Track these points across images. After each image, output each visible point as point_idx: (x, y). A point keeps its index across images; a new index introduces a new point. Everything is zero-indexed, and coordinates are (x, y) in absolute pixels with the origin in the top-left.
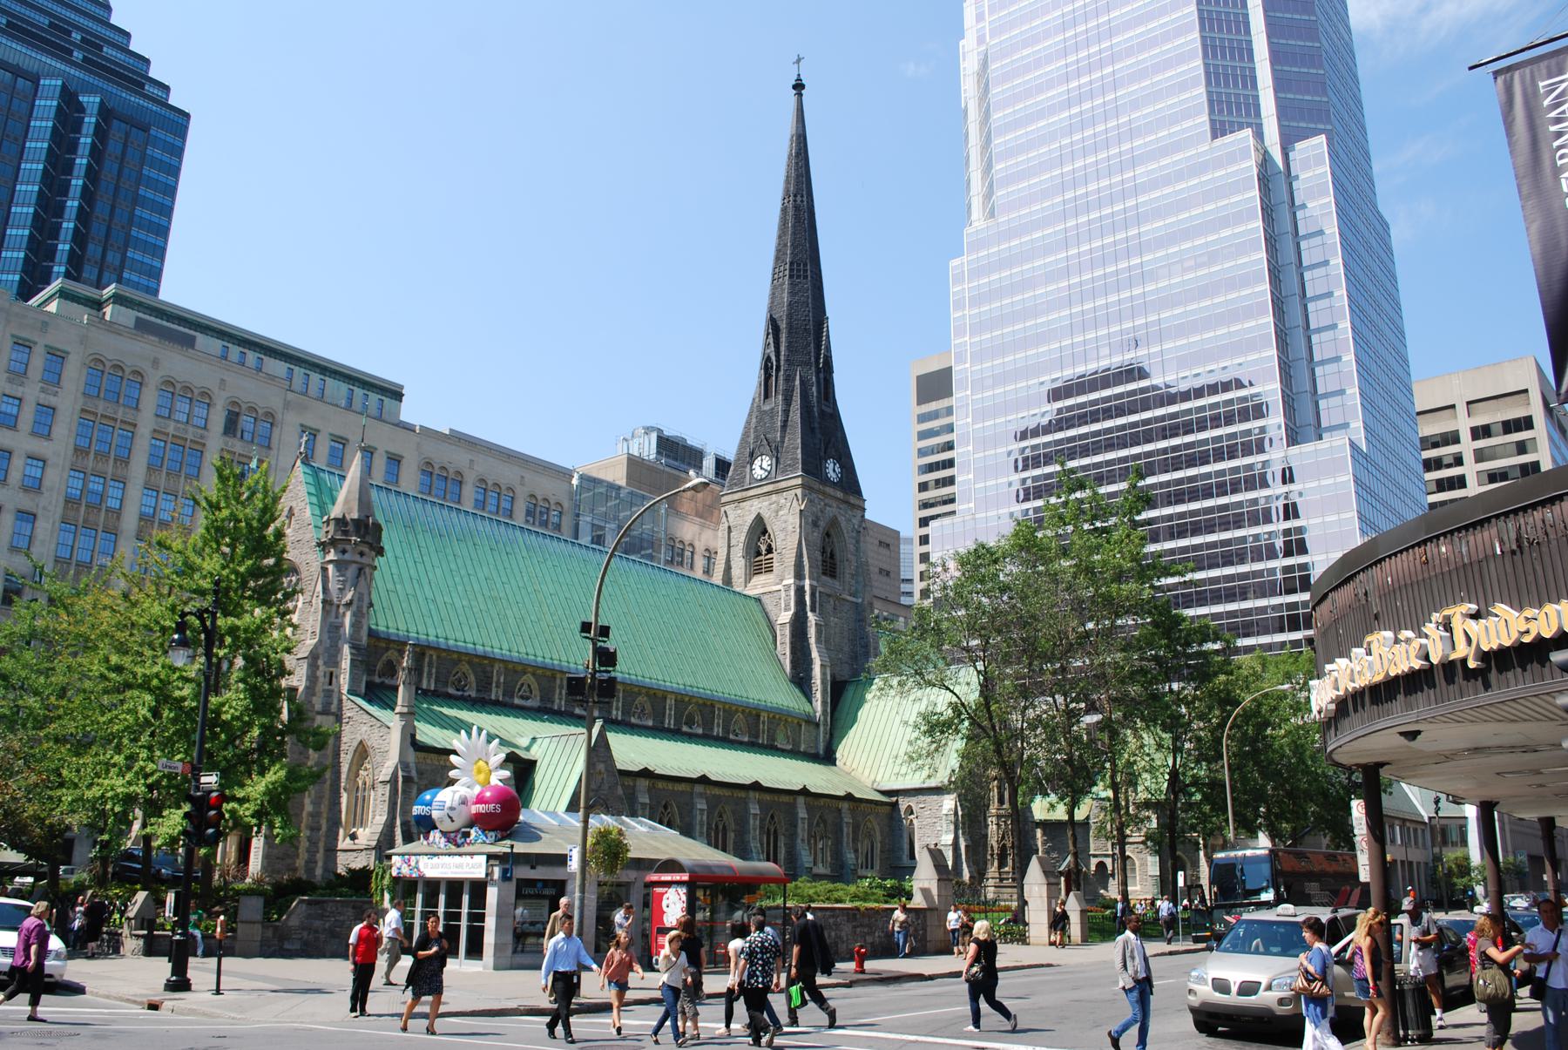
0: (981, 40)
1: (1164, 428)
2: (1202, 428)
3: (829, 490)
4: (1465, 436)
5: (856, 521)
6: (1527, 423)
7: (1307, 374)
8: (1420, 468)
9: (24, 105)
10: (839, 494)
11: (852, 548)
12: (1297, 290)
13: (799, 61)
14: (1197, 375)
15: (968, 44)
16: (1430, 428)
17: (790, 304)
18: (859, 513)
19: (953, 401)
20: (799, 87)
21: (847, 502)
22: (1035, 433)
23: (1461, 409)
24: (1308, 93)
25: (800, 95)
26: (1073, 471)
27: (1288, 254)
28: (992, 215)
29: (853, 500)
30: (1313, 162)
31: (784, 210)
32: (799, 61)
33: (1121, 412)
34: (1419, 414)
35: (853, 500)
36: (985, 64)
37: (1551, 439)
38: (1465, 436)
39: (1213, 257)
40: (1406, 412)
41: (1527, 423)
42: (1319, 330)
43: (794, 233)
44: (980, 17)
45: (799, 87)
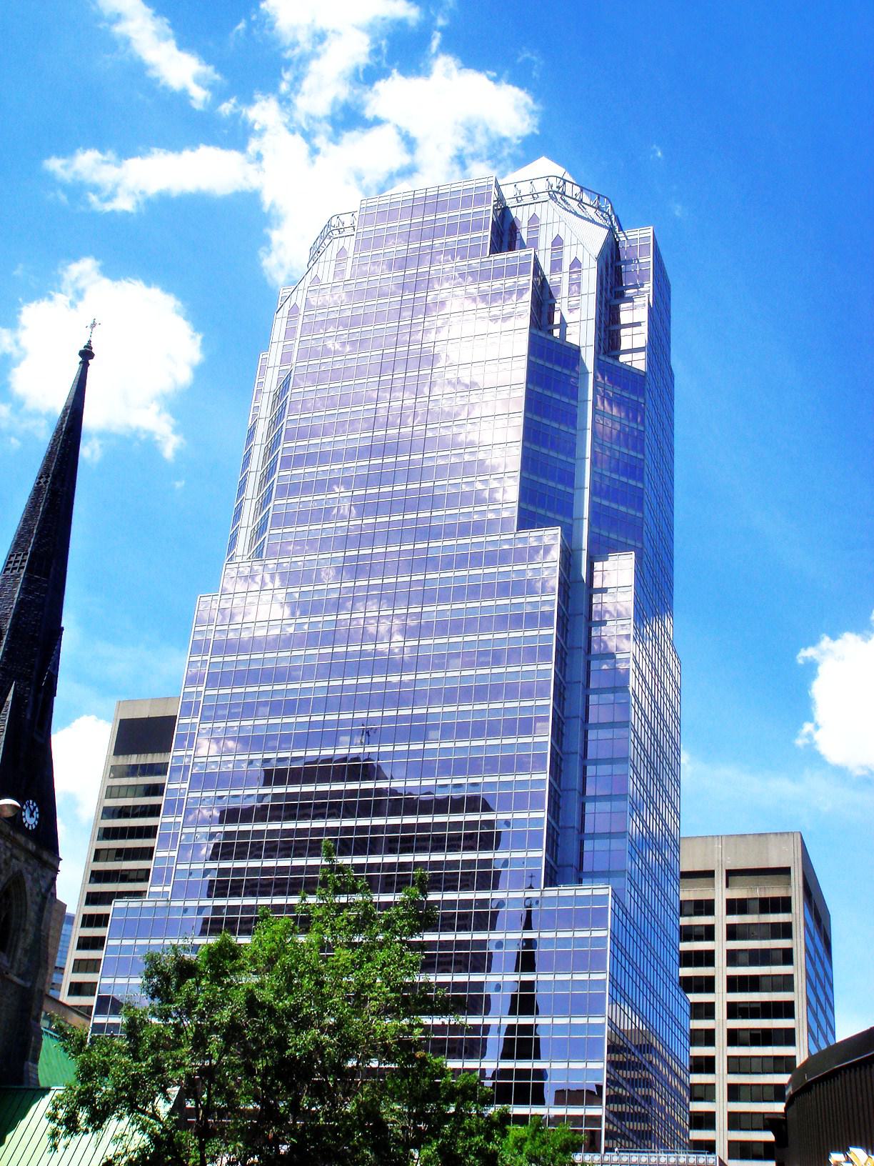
0: (286, 358)
1: (394, 840)
2: (454, 848)
3: (21, 838)
4: (720, 907)
5: (43, 884)
6: (783, 905)
7: (577, 806)
8: (676, 936)
9: (488, 368)
10: (31, 846)
11: (32, 915)
12: (581, 712)
13: (93, 325)
14: (459, 786)
15: (274, 355)
16: (691, 893)
17: (21, 604)
18: (50, 874)
19: (169, 759)
20: (87, 355)
21: (39, 858)
22: (246, 815)
23: (720, 878)
24: (623, 504)
25: (85, 366)
26: (341, 869)
27: (578, 673)
28: (259, 554)
29: (45, 856)
30: (617, 575)
31: (38, 490)
32: (93, 325)
33: (349, 811)
34: (685, 875)
35: (45, 856)
36: (285, 386)
37: (806, 925)
38: (720, 907)
39: (497, 659)
40: (671, 870)
41: (783, 905)
42: (596, 762)
43: (43, 520)
44: (289, 333)
45: (87, 355)
